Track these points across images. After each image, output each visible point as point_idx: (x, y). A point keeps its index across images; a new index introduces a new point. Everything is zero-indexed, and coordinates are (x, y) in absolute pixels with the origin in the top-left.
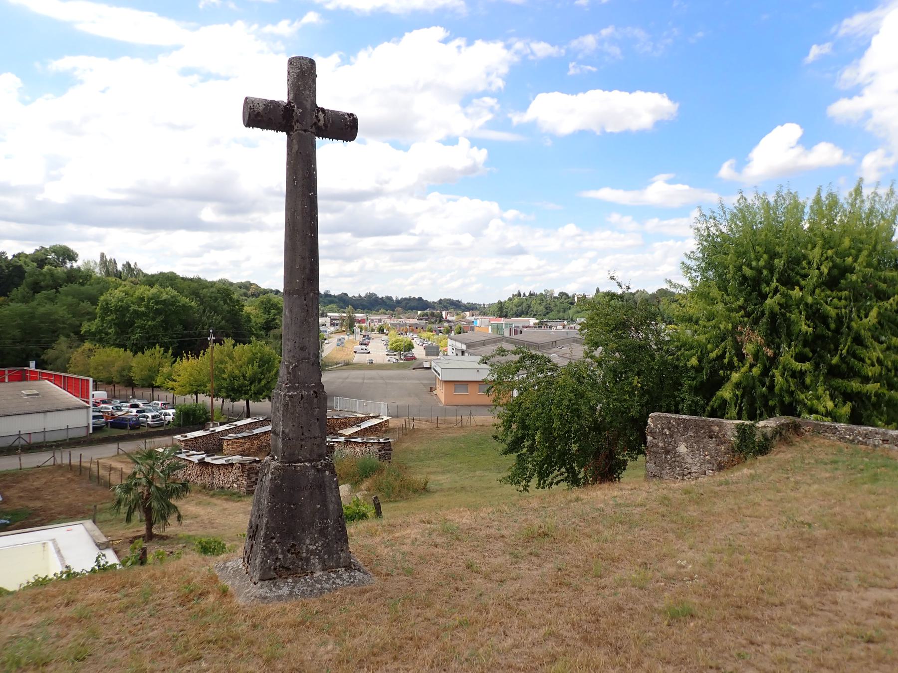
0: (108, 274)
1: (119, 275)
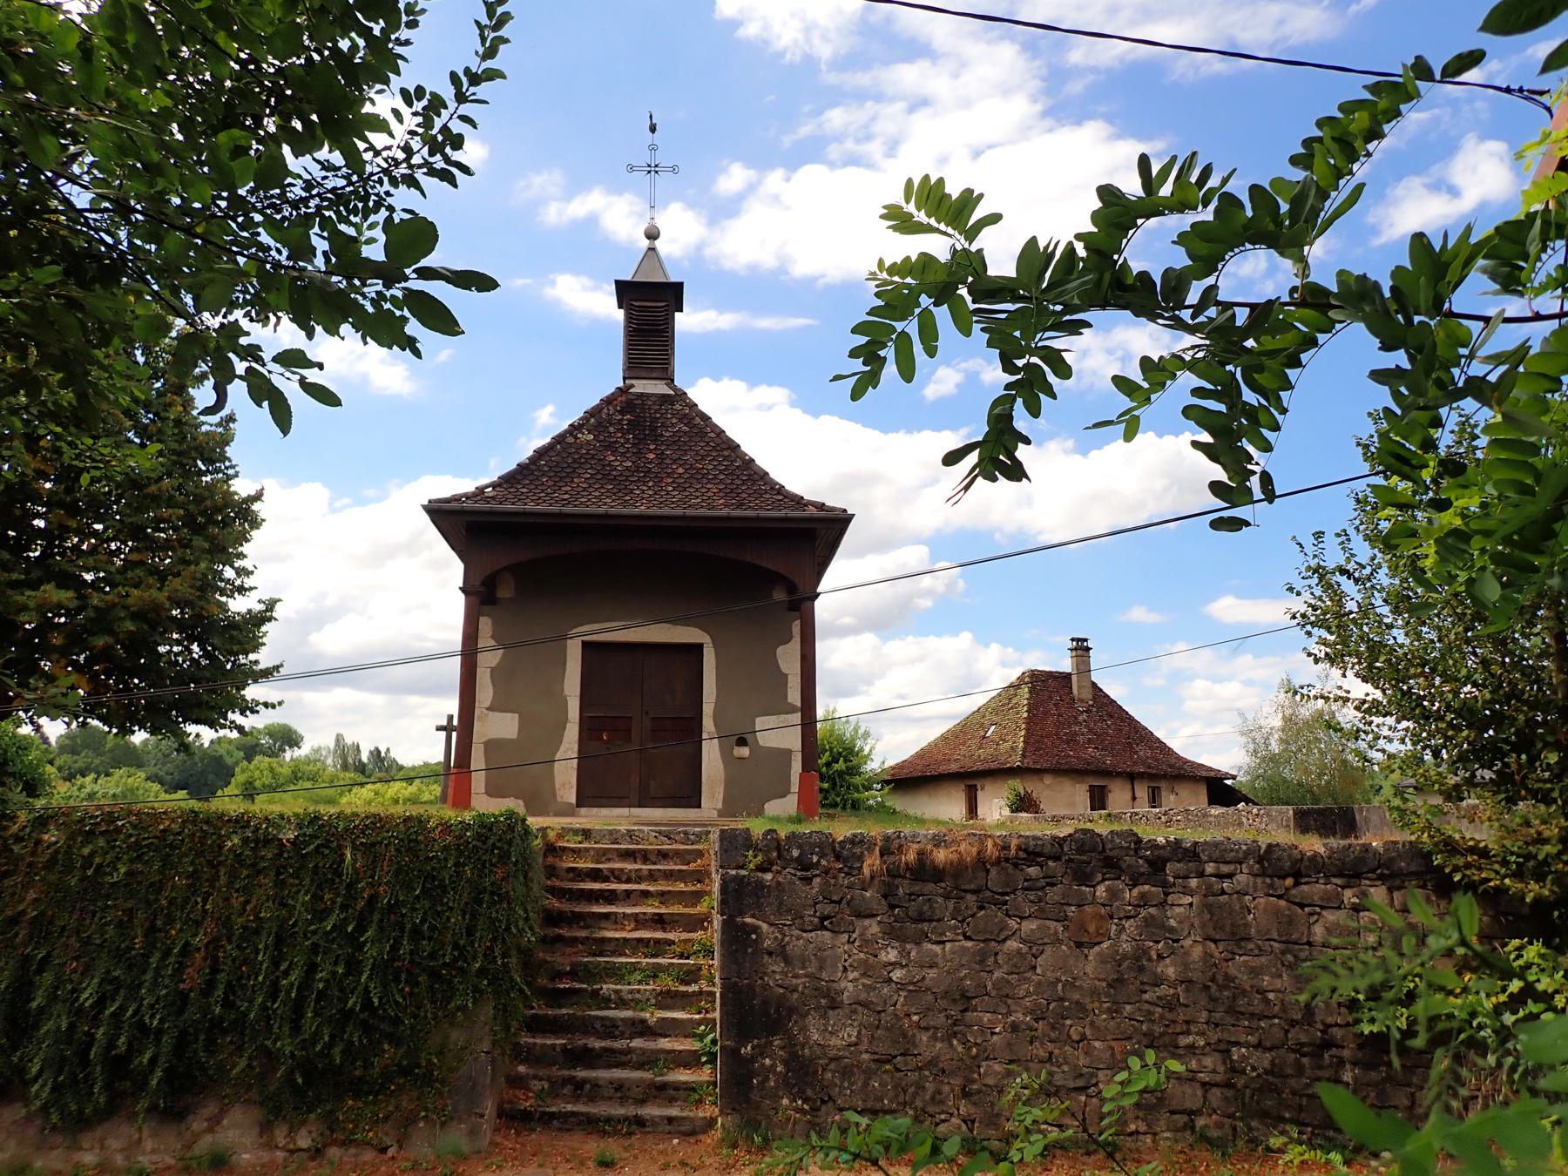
0: (345, 767)
1: (361, 768)
